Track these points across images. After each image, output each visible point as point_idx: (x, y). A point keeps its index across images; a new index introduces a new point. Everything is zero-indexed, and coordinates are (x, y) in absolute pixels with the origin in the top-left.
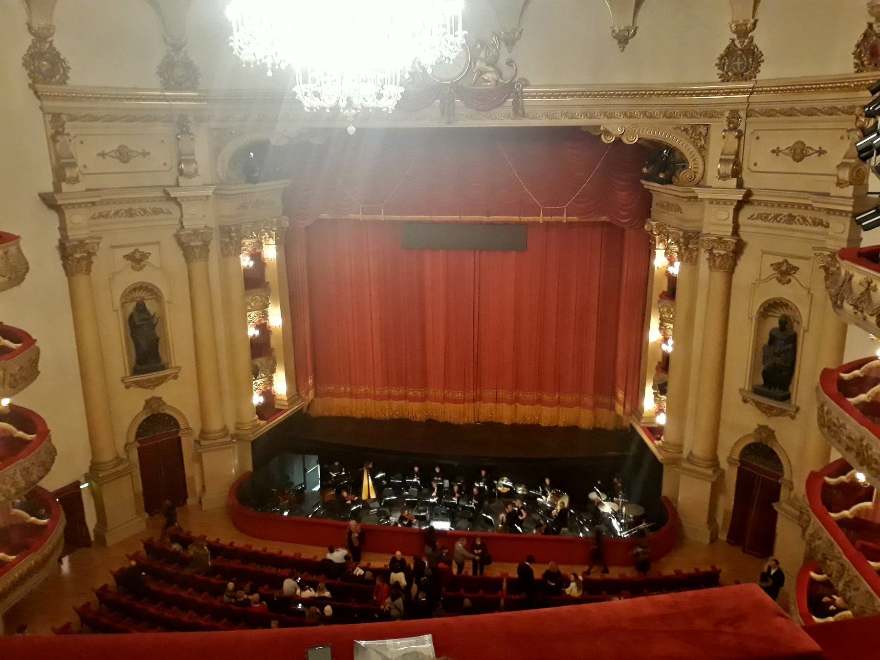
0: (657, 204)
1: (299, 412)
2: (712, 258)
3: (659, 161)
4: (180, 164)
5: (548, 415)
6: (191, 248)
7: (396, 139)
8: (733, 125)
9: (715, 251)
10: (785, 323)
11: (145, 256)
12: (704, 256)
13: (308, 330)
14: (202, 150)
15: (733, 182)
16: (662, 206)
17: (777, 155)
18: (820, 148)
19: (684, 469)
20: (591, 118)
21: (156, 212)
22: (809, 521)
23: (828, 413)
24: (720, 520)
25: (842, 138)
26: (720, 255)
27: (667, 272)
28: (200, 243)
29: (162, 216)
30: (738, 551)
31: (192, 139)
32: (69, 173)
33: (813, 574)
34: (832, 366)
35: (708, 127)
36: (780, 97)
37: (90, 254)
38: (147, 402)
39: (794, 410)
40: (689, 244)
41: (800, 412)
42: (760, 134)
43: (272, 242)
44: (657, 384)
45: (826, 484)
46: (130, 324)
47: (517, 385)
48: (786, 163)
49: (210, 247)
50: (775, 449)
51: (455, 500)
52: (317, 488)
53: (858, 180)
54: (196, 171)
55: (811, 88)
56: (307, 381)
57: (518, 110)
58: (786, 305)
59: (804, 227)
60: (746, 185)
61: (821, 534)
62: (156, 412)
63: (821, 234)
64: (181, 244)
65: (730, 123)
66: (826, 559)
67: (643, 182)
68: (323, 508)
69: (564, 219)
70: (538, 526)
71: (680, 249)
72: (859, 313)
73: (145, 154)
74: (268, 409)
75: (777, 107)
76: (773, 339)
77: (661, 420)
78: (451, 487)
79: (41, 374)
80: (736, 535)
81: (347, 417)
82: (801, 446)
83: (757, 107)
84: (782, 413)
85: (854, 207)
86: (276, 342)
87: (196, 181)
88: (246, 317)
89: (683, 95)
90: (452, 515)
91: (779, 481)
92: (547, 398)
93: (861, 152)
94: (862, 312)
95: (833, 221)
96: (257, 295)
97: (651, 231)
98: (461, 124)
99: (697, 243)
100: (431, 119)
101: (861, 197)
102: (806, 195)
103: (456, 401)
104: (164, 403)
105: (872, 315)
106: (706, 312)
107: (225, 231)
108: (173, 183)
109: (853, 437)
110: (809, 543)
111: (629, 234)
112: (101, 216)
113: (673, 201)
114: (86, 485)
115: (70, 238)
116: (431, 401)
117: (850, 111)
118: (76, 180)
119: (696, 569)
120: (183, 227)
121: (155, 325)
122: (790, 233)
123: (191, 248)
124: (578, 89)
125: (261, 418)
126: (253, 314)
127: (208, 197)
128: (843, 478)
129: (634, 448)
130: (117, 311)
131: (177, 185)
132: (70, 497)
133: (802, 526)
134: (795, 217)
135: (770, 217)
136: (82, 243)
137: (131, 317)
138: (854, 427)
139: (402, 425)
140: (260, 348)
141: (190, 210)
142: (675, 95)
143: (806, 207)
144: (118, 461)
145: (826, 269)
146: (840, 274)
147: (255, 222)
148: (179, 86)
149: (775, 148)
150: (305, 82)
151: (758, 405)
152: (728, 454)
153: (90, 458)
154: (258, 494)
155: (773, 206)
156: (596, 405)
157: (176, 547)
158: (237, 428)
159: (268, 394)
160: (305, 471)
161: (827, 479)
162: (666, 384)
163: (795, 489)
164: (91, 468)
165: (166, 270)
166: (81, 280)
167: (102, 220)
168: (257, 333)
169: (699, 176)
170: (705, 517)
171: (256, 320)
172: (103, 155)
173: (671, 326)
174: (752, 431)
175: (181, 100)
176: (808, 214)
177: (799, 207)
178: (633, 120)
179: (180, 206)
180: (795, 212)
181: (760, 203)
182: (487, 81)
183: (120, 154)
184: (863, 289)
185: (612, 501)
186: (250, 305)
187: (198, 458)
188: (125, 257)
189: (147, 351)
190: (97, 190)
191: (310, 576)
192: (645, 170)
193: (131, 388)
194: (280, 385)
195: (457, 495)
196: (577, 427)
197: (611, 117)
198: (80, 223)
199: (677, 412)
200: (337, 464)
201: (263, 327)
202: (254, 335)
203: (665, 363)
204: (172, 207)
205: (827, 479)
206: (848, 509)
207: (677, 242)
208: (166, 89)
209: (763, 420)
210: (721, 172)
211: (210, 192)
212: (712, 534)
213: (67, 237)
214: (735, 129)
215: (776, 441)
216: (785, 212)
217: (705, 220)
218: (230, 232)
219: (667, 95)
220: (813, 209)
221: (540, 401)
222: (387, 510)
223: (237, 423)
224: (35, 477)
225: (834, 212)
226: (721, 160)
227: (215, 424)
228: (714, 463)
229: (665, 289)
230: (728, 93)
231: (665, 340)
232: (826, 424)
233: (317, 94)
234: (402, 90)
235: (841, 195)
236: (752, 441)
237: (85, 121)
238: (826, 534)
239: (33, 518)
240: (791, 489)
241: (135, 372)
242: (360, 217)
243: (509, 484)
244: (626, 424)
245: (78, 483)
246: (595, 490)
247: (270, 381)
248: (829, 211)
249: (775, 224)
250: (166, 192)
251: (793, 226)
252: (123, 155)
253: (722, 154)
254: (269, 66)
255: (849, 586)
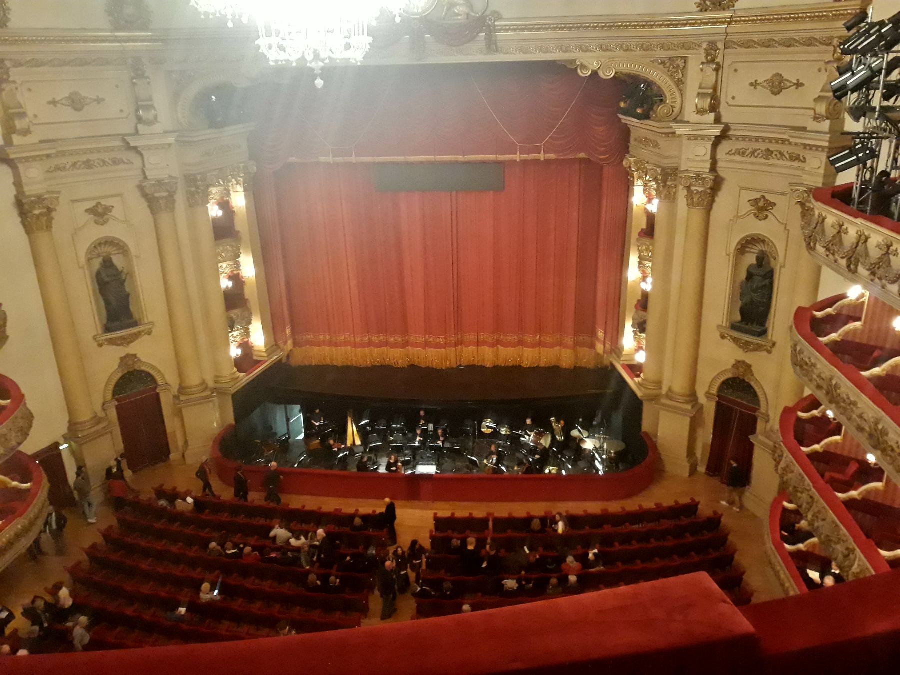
0: (636, 140)
1: (279, 363)
2: (690, 194)
3: (636, 96)
4: (137, 110)
5: (530, 356)
6: (156, 200)
7: (366, 77)
8: (711, 59)
9: (693, 188)
10: (762, 260)
11: (108, 209)
12: (682, 193)
13: (283, 284)
14: (161, 98)
15: (711, 117)
16: (641, 142)
17: (755, 88)
18: (798, 80)
19: (663, 405)
20: (566, 52)
21: (116, 162)
22: (782, 456)
23: (801, 352)
24: (699, 453)
25: (820, 70)
26: (698, 192)
27: (646, 209)
28: (165, 194)
29: (122, 166)
30: (715, 482)
31: (149, 83)
32: (19, 124)
33: (786, 504)
34: (805, 303)
35: (685, 59)
36: (758, 27)
37: (50, 210)
38: (122, 359)
39: (771, 345)
40: (667, 179)
41: (777, 345)
42: (739, 66)
43: (240, 189)
44: (636, 322)
45: (799, 419)
46: (98, 281)
47: (498, 328)
48: (764, 97)
49: (176, 197)
50: (753, 384)
51: (440, 443)
52: (301, 437)
53: (834, 116)
54: (156, 117)
55: (790, 18)
56: (285, 331)
57: (492, 45)
58: (764, 242)
59: (781, 162)
60: (724, 120)
61: (793, 468)
62: (131, 370)
63: (797, 169)
64: (145, 196)
65: (708, 55)
66: (797, 491)
67: (621, 116)
68: (309, 456)
69: (542, 157)
70: (520, 464)
71: (658, 185)
72: (831, 256)
73: (99, 101)
74: (246, 361)
75: (756, 38)
76: (750, 276)
77: (641, 358)
78: (436, 430)
79: (9, 342)
80: (715, 467)
81: (328, 366)
82: (777, 381)
83: (735, 38)
84: (758, 348)
85: (830, 142)
86: (251, 292)
87: (158, 128)
88: (218, 270)
89: (660, 26)
90: (438, 457)
91: (757, 414)
92: (529, 339)
93: (835, 92)
94: (833, 254)
95: (808, 154)
96: (227, 247)
97: (630, 167)
98: (431, 61)
99: (675, 180)
100: (401, 57)
101: (838, 133)
102: (784, 130)
103: (437, 346)
104: (140, 360)
105: (843, 258)
106: (684, 245)
107: (191, 180)
108: (133, 131)
109: (823, 376)
110: (782, 477)
111: (608, 172)
112: (58, 169)
113: (650, 136)
114: (66, 446)
115: (27, 194)
116: (412, 346)
117: (828, 42)
118: (26, 132)
119: (677, 503)
120: (146, 178)
121: (124, 281)
122: (769, 169)
123: (156, 200)
124: (552, 22)
125: (240, 371)
126: (224, 265)
127: (170, 145)
128: (815, 413)
129: (613, 384)
130: (83, 268)
131: (137, 132)
132: (50, 459)
133: (775, 460)
134: (772, 152)
135: (748, 152)
136: (40, 199)
137: (98, 274)
138: (824, 367)
139: (384, 371)
140: (235, 300)
141: (151, 159)
142: (652, 26)
143: (784, 141)
144: (96, 420)
145: (802, 204)
146: (814, 215)
147: (221, 169)
148: (129, 25)
149: (753, 81)
150: (269, 35)
151: (736, 340)
152: (706, 389)
153: (67, 419)
154: (241, 444)
155: (750, 141)
156: (577, 344)
157: (163, 503)
158: (216, 382)
159: (246, 347)
160: (288, 420)
161: (800, 414)
162: (645, 322)
163: (771, 422)
164: (70, 429)
165: (131, 224)
166: (43, 239)
167: (59, 173)
168: (230, 284)
169: (677, 110)
170: (684, 453)
171: (228, 271)
172: (54, 103)
173: (650, 264)
174: (730, 367)
175: (134, 41)
176: (785, 149)
177: (777, 142)
178: (609, 54)
179: (142, 155)
180: (773, 147)
181: (737, 138)
182: (458, 15)
183: (73, 102)
184: (835, 232)
185: (594, 437)
186: (221, 256)
187: (179, 414)
188: (87, 211)
189: (118, 310)
190: (54, 141)
191: (299, 526)
192: (622, 105)
193: (104, 347)
194: (258, 337)
195: (442, 439)
196: (558, 367)
197: (587, 50)
198: (36, 179)
199: (656, 350)
200: (318, 411)
201: (236, 278)
202: (227, 287)
203: (644, 302)
204: (132, 156)
205: (800, 414)
206: (818, 443)
207: (656, 180)
208: (117, 29)
209: (741, 355)
210: (699, 107)
211: (171, 140)
212: (691, 466)
213: (24, 192)
214: (713, 61)
215: (753, 375)
216: (763, 147)
217: (684, 157)
218: (195, 181)
219: (644, 26)
220: (790, 144)
221: (521, 343)
222: (373, 456)
223: (217, 377)
224: (14, 443)
225: (811, 147)
226: (699, 94)
227: (193, 380)
228: (692, 397)
229: (644, 226)
230: (706, 24)
231: (644, 279)
232: (801, 365)
233: (282, 49)
234: (370, 40)
235: (816, 129)
236: (730, 376)
237: (32, 67)
238: (798, 469)
239: (15, 483)
240: (768, 422)
241: (107, 330)
242: (330, 159)
243: (493, 425)
244: (606, 362)
245: (57, 445)
246: (576, 428)
247: (247, 333)
248: (805, 146)
249: (753, 160)
250: (124, 140)
251: (771, 162)
252: (76, 103)
253: (700, 88)
254: (229, 17)
255: (817, 517)
